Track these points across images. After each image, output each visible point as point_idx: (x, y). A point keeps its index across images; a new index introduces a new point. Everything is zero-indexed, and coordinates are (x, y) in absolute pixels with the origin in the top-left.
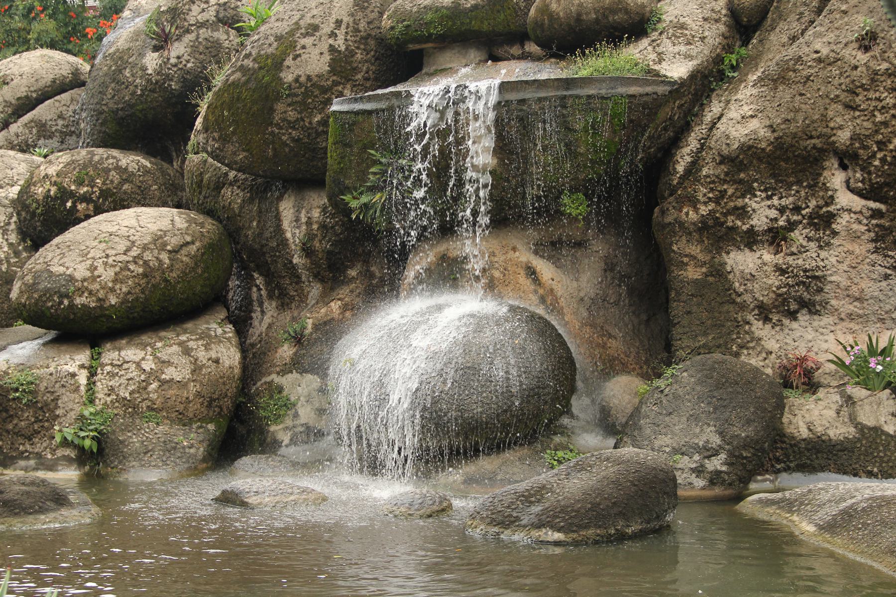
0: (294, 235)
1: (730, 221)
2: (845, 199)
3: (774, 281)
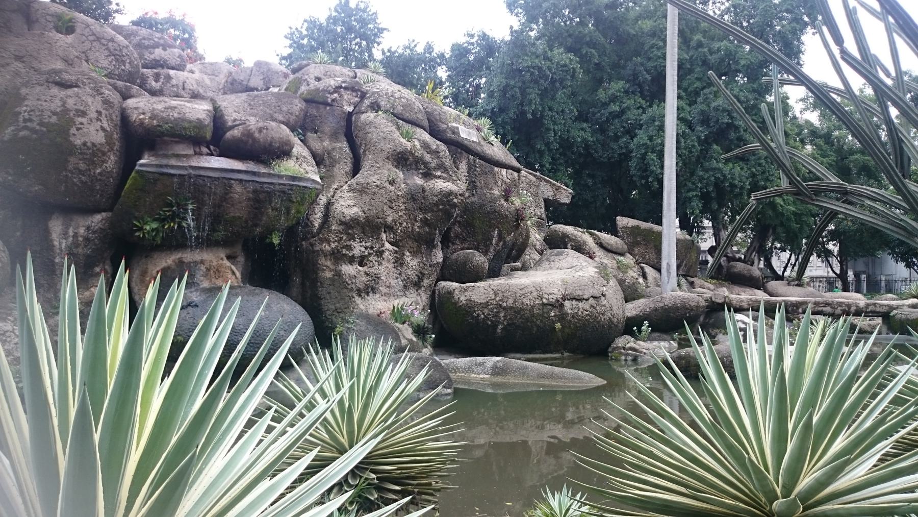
0: (60, 244)
1: (344, 251)
3: (365, 278)
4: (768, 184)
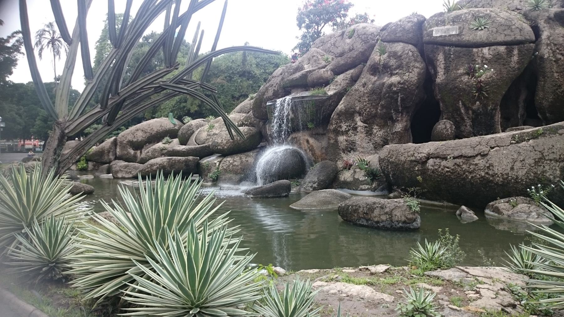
2: (360, 123)
3: (345, 143)
4: (119, 131)
